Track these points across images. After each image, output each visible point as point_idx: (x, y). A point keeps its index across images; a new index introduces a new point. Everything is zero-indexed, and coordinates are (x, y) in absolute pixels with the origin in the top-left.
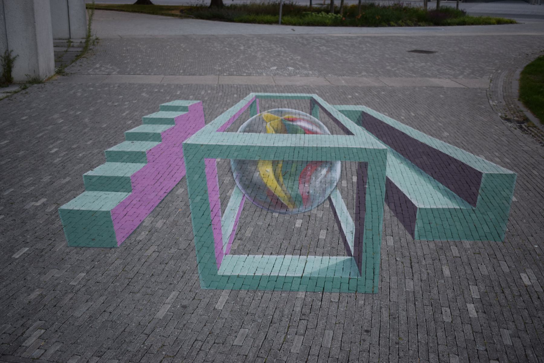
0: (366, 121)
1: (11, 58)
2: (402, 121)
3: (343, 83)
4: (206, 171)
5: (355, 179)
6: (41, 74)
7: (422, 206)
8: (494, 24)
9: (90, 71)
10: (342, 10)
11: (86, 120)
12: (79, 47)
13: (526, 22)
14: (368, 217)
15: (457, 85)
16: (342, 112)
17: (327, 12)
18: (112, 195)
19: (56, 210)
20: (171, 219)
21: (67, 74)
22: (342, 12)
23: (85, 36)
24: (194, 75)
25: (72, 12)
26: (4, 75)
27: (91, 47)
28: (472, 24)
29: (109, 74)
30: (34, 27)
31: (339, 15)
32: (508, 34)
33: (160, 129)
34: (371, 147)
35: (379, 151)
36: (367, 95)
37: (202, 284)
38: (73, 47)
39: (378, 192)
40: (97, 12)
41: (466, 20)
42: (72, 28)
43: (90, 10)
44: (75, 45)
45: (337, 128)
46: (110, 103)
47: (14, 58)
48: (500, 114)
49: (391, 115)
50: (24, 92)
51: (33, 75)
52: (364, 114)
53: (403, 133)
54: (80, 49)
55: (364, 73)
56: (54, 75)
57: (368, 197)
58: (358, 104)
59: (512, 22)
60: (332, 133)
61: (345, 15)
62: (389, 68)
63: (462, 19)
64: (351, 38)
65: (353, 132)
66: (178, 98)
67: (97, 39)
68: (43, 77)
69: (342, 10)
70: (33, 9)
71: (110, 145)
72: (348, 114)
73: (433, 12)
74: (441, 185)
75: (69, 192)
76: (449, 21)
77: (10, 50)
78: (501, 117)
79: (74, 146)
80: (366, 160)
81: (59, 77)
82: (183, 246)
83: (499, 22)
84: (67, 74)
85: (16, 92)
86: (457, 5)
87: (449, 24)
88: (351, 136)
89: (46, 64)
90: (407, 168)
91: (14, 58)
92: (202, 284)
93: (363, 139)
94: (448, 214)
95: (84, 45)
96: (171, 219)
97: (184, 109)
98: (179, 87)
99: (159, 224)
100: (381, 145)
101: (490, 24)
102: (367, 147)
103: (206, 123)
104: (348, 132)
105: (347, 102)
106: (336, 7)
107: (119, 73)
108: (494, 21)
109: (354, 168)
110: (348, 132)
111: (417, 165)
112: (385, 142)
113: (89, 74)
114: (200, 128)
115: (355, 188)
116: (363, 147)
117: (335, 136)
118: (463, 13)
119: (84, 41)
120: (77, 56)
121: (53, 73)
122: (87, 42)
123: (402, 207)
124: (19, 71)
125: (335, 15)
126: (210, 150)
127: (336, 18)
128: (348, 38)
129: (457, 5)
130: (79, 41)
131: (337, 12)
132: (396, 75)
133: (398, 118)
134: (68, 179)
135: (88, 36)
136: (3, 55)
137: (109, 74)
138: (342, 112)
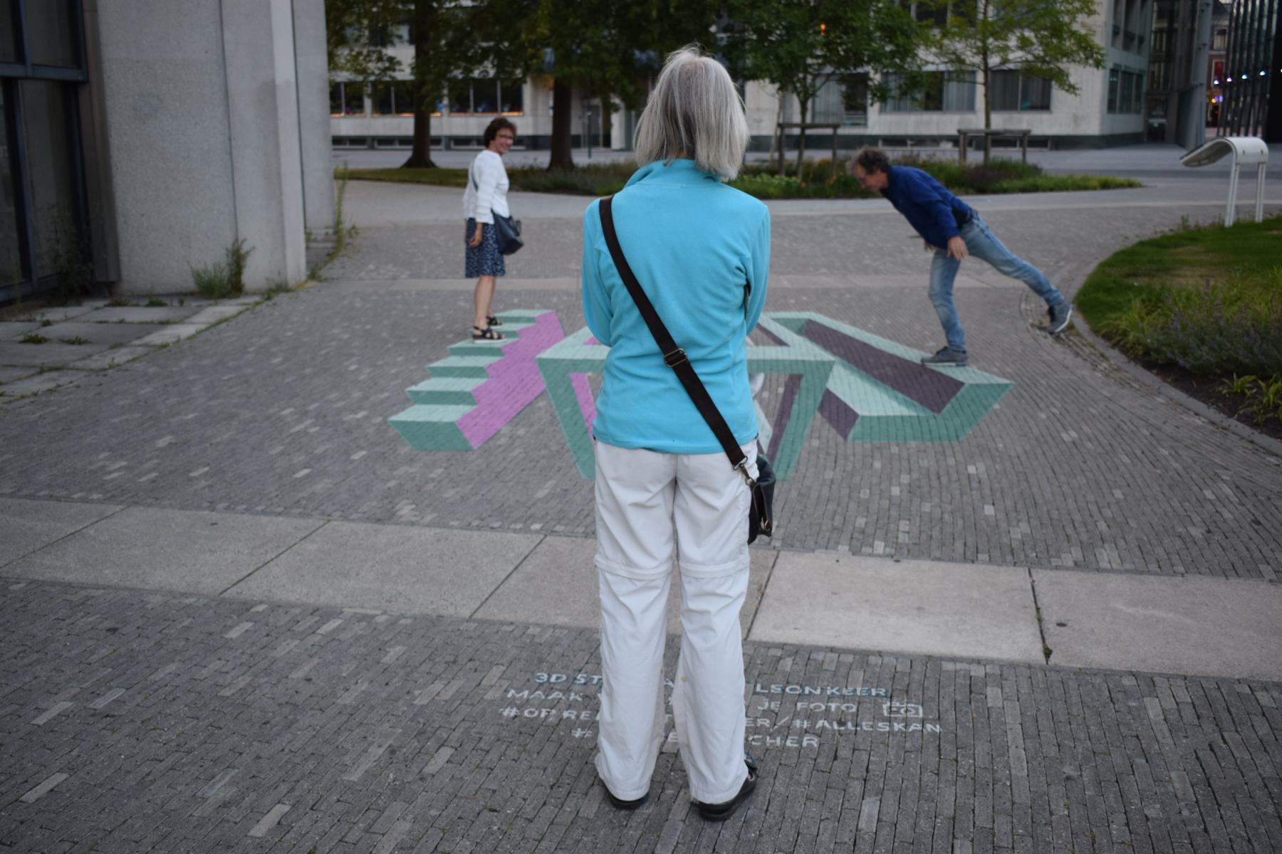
0: (812, 332)
1: (243, 251)
2: (869, 330)
3: (786, 284)
4: (574, 384)
5: (781, 390)
6: (289, 277)
7: (866, 413)
8: (1094, 188)
9: (362, 274)
10: (801, 169)
11: (384, 335)
12: (325, 241)
13: (1161, 184)
14: (790, 426)
15: (978, 284)
16: (777, 320)
17: (772, 173)
18: (451, 408)
19: (385, 422)
20: (536, 427)
21: (326, 280)
22: (800, 175)
23: (331, 223)
24: (536, 277)
25: (308, 182)
26: (229, 280)
27: (349, 241)
28: (1051, 190)
29: (394, 278)
30: (281, 203)
31: (794, 179)
32: (1108, 205)
33: (467, 385)
34: (812, 359)
35: (823, 363)
36: (821, 298)
37: (583, 476)
38: (315, 241)
39: (811, 402)
40: (352, 184)
41: (1039, 181)
42: (309, 209)
43: (340, 182)
44: (319, 238)
45: (765, 337)
46: (412, 315)
47: (248, 253)
48: (1031, 321)
49: (853, 323)
50: (270, 303)
51: (277, 279)
52: (810, 322)
53: (865, 344)
54: (329, 245)
55: (824, 270)
56: (306, 282)
57: (795, 407)
58: (803, 310)
59: (1131, 185)
60: (757, 344)
61: (805, 179)
62: (868, 262)
63: (1030, 181)
64: (812, 218)
65: (788, 341)
66: (518, 306)
67: (353, 228)
68: (291, 283)
69: (801, 169)
70: (279, 174)
71: (431, 361)
72: (786, 323)
73: (978, 168)
74: (900, 395)
75: (394, 405)
76: (1005, 185)
77: (240, 239)
78: (1032, 325)
79: (380, 363)
80: (802, 372)
81: (312, 284)
82: (554, 448)
83: (1105, 186)
84: (326, 280)
85: (257, 303)
86: (1024, 155)
87: (1005, 191)
88: (785, 348)
89: (296, 264)
90: (859, 380)
91: (248, 253)
92: (583, 476)
93: (803, 350)
94: (899, 421)
95: (334, 238)
96: (536, 427)
97: (529, 320)
98: (518, 294)
99: (521, 432)
100: (826, 356)
101: (1086, 188)
102: (806, 358)
103: (566, 335)
104: (780, 342)
105: (785, 308)
106: (790, 165)
107: (412, 276)
108: (1095, 183)
109: (783, 380)
110: (780, 342)
111: (874, 376)
112: (834, 353)
113: (361, 279)
114: (556, 341)
115: (780, 399)
116: (800, 358)
117: (761, 348)
118: (1036, 170)
119: (331, 231)
120: (329, 255)
121: (304, 278)
122: (337, 232)
123: (839, 414)
124: (254, 275)
125: (786, 179)
126: (575, 365)
127: (788, 184)
128: (805, 218)
129: (1024, 155)
130: (324, 231)
131: (790, 174)
132: (877, 272)
133: (864, 327)
134: (386, 394)
135: (338, 223)
136: (230, 247)
137: (394, 278)
138: (777, 320)
